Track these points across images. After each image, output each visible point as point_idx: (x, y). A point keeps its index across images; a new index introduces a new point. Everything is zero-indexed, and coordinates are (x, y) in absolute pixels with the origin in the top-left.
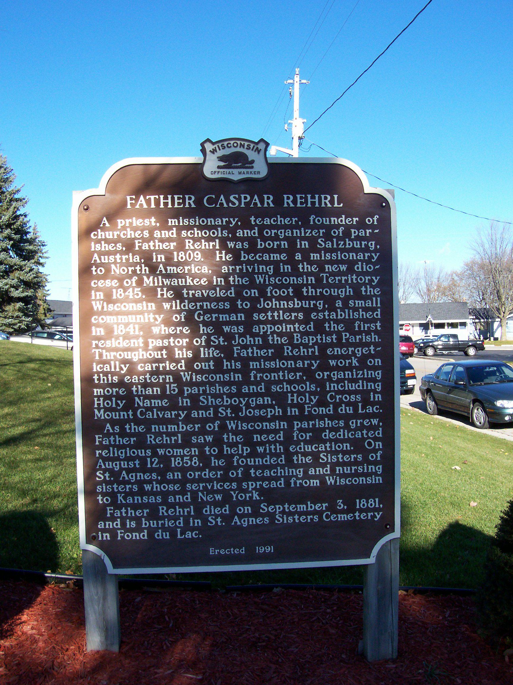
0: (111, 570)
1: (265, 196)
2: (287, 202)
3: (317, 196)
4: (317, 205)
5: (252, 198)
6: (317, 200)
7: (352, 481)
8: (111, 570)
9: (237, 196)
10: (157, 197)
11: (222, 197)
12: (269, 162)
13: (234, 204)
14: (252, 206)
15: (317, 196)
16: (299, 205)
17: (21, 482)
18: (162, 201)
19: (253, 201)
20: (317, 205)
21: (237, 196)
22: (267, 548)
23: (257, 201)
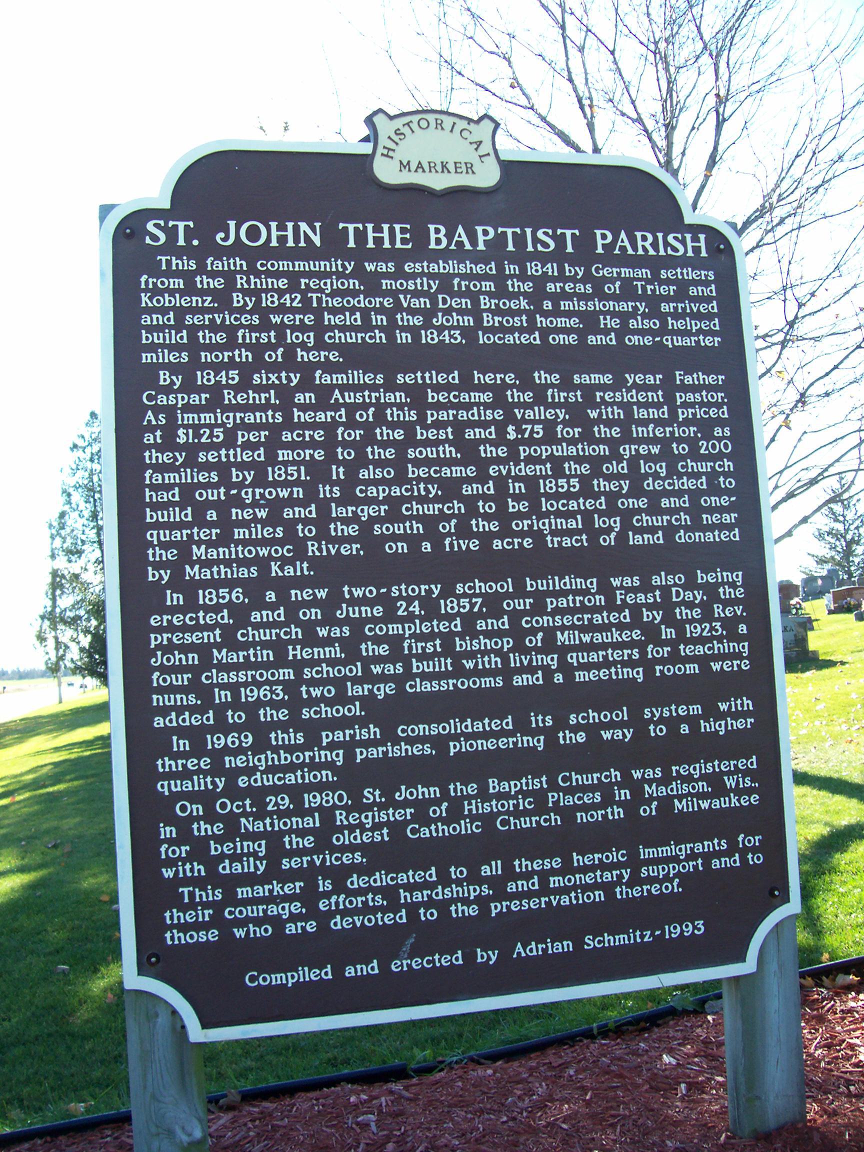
0: (196, 1033)
1: (639, 235)
2: (643, 246)
3: (386, 227)
4: (387, 245)
5: (616, 238)
6: (386, 235)
7: (531, 622)
8: (196, 1033)
9: (679, 236)
10: (360, 226)
11: (460, 230)
12: (502, 158)
13: (675, 250)
14: (617, 252)
15: (386, 227)
16: (398, 245)
17: (28, 1107)
18: (371, 235)
19: (619, 244)
20: (387, 245)
21: (550, 231)
22: (314, 797)
23: (464, 238)
